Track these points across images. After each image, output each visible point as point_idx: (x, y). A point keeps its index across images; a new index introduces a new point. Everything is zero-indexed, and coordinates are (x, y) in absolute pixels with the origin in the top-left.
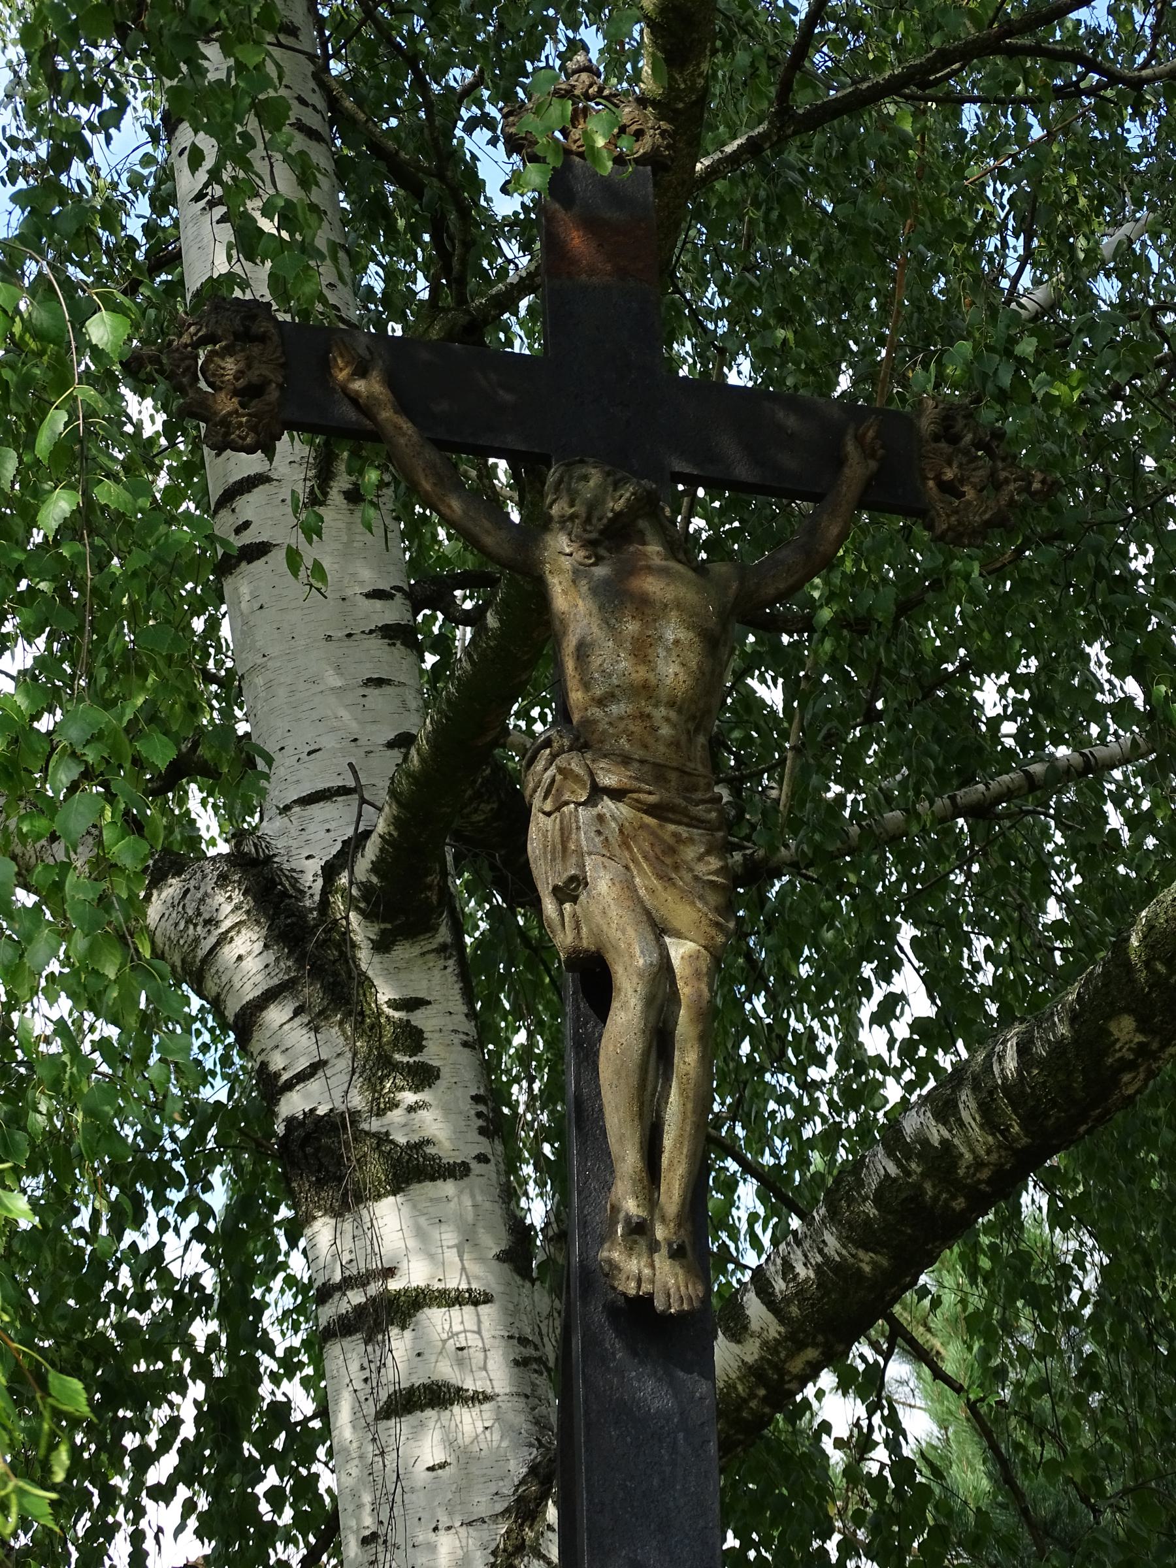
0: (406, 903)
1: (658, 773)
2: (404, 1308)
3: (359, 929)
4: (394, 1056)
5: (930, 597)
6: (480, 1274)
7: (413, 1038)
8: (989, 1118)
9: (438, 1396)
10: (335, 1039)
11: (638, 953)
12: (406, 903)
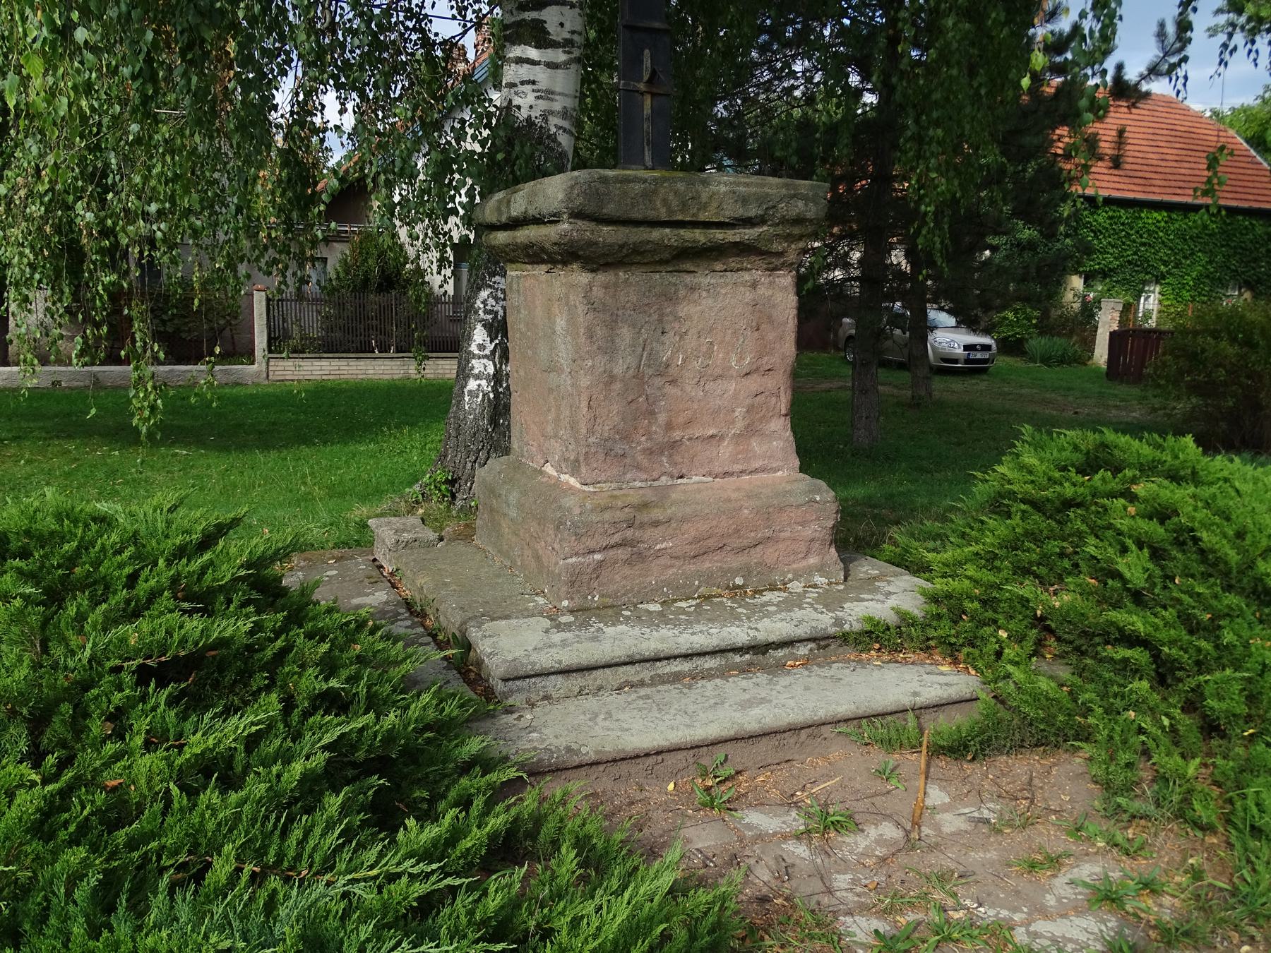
5: (601, 361)
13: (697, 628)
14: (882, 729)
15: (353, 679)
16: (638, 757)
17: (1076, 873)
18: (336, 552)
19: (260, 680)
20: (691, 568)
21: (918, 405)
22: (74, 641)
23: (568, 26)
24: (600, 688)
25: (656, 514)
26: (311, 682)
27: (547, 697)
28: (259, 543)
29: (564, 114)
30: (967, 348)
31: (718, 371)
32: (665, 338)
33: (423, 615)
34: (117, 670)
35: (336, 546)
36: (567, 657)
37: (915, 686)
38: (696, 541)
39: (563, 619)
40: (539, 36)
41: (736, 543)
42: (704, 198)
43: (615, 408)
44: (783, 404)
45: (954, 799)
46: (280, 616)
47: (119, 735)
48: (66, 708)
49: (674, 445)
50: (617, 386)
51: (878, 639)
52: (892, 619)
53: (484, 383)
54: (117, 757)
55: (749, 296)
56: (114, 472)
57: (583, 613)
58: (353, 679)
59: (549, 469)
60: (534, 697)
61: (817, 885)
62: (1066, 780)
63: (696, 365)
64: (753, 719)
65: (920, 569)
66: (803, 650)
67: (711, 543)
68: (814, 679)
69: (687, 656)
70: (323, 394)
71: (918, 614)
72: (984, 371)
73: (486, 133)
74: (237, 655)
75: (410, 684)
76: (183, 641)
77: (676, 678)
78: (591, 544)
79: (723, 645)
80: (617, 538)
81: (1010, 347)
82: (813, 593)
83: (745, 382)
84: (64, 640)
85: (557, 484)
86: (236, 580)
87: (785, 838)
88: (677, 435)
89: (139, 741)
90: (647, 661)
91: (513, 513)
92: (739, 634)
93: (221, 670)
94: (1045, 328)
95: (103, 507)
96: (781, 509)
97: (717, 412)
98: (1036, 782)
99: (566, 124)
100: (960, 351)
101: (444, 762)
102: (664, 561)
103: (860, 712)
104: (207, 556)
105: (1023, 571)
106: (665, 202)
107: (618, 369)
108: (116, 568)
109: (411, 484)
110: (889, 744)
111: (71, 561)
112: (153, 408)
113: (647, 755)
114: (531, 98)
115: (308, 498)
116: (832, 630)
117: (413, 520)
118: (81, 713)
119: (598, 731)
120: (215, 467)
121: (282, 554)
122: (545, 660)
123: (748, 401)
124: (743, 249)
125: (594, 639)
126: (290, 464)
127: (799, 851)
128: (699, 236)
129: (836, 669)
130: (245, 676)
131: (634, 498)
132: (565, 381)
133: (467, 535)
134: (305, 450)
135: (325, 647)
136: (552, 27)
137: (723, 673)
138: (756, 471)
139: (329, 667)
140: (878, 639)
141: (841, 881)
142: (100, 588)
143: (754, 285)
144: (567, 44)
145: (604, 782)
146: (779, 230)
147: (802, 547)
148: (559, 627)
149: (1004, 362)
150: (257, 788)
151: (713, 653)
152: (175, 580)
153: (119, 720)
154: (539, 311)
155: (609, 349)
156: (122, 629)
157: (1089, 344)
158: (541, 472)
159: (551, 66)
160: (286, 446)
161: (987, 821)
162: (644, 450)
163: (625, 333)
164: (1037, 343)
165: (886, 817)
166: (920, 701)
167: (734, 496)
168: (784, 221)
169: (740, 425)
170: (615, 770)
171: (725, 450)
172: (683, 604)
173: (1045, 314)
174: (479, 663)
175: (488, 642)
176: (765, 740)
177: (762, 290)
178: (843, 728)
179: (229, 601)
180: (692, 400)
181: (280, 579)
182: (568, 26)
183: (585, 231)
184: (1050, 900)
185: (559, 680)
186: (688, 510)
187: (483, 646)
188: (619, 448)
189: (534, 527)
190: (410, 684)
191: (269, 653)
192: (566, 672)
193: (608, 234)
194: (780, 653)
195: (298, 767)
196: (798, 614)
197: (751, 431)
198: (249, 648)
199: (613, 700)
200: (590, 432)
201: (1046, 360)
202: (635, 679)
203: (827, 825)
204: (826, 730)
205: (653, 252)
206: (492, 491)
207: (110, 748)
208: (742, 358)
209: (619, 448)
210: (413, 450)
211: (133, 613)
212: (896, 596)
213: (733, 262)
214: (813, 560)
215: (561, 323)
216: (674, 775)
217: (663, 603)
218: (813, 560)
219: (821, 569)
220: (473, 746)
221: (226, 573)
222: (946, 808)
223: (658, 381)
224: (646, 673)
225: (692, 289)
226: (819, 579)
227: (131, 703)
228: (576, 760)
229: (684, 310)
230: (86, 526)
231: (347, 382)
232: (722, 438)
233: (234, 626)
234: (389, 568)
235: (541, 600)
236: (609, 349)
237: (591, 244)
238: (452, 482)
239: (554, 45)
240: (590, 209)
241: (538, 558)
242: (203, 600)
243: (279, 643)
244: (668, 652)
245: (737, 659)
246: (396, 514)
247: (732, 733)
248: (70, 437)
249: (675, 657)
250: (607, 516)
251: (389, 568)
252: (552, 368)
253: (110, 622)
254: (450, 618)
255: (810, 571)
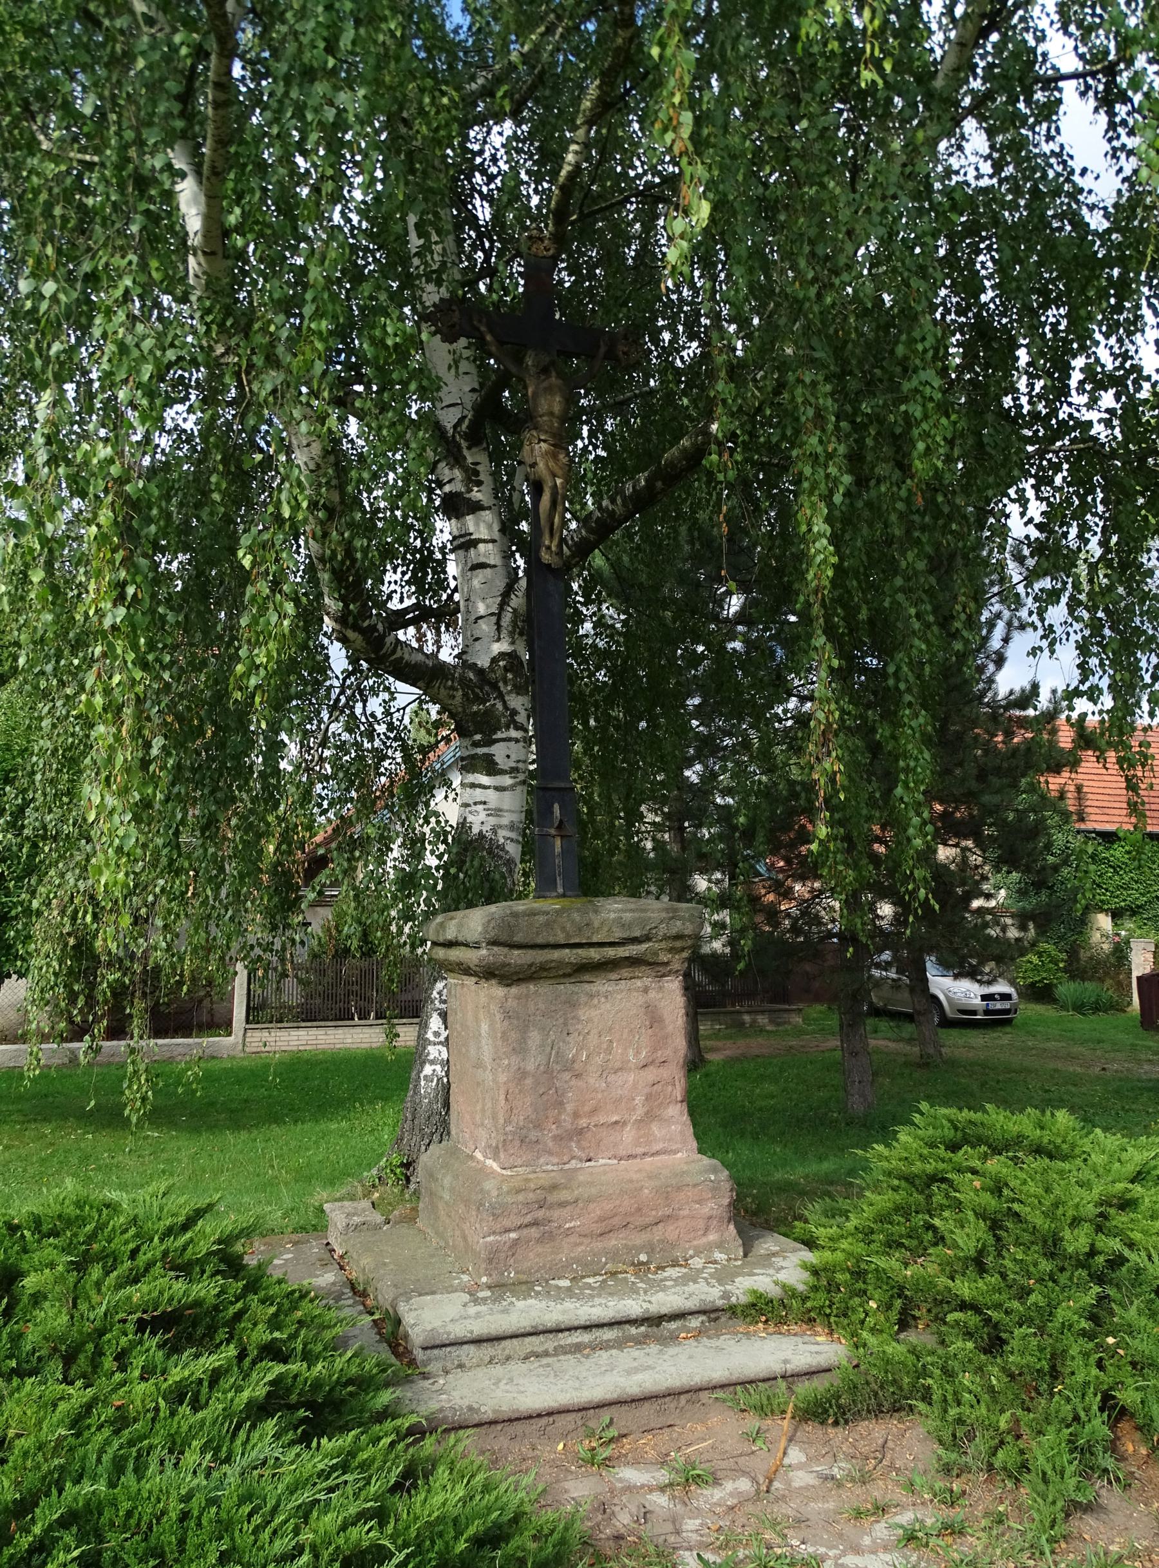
0: (475, 437)
1: (554, 435)
2: (474, 543)
3: (464, 444)
4: (472, 477)
5: (515, 1060)
6: (496, 535)
7: (477, 473)
8: (624, 504)
9: (483, 566)
10: (457, 473)
11: (972, 1115)
12: (475, 437)
13: (597, 1301)
14: (750, 1394)
15: (293, 1336)
16: (530, 1417)
17: (899, 1519)
18: (295, 1237)
19: (221, 1334)
20: (598, 1245)
21: (927, 1065)
22: (95, 1298)
23: (514, 757)
24: (508, 1358)
25: (564, 1195)
26: (262, 1335)
27: (461, 1366)
28: (229, 1222)
29: (512, 827)
30: (984, 998)
31: (618, 1065)
32: (570, 1039)
33: (364, 1294)
34: (124, 1321)
35: (295, 1231)
36: (479, 1328)
37: (788, 1354)
38: (601, 1219)
39: (481, 1294)
40: (491, 768)
41: (640, 1221)
42: (596, 924)
43: (528, 1101)
44: (678, 1092)
45: (809, 1459)
46: (240, 1284)
47: (123, 1368)
48: (90, 1347)
49: (580, 1132)
50: (529, 1081)
51: (762, 1311)
52: (774, 1292)
53: (438, 1068)
54: (123, 1383)
55: (641, 999)
56: (87, 1158)
57: (499, 1288)
58: (293, 1336)
59: (478, 1155)
60: (449, 1365)
61: (669, 1527)
62: (912, 1442)
63: (598, 1060)
64: (635, 1384)
65: (810, 1243)
66: (695, 1322)
67: (616, 1221)
68: (701, 1349)
69: (587, 1328)
70: (299, 1068)
71: (801, 1288)
72: (1008, 1022)
73: (442, 847)
74: (208, 1313)
75: (340, 1344)
76: (171, 1299)
77: (578, 1348)
78: (507, 1223)
79: (619, 1317)
80: (528, 1219)
81: (1040, 993)
82: (711, 1269)
83: (643, 1073)
84: (88, 1298)
85: (482, 1171)
86: (209, 1254)
87: (651, 1490)
88: (583, 1122)
89: (137, 1373)
90: (550, 1331)
91: (447, 1196)
92: (633, 1307)
93: (194, 1325)
94: (1076, 971)
95: (113, 1195)
96: (679, 1189)
97: (619, 1100)
98: (890, 1444)
99: (513, 835)
100: (978, 1001)
101: (362, 1411)
102: (573, 1239)
103: (734, 1378)
104: (188, 1235)
105: (893, 1244)
106: (563, 929)
107: (530, 1066)
108: (122, 1245)
109: (369, 1167)
110: (762, 1410)
111: (92, 1237)
112: (144, 1099)
113: (539, 1416)
114: (482, 816)
115: (272, 1183)
116: (720, 1303)
117: (365, 1204)
118: (99, 1353)
119: (499, 1393)
120: (185, 1149)
121: (246, 1233)
122: (459, 1331)
123: (647, 1090)
124: (634, 962)
125: (505, 1311)
126: (259, 1145)
127: (660, 1501)
128: (594, 954)
129: (722, 1341)
130: (212, 1330)
131: (544, 1180)
132: (488, 1076)
133: (411, 1218)
134: (276, 1130)
135: (272, 1310)
136: (500, 759)
137: (620, 1344)
138: (657, 1153)
139: (274, 1323)
140: (762, 1311)
141: (691, 1524)
142: (110, 1261)
143: (646, 990)
144: (513, 771)
145: (499, 1440)
146: (663, 945)
147: (701, 1224)
148: (476, 1301)
149: (1032, 1011)
150: (215, 1408)
151: (611, 1324)
152: (165, 1254)
153: (122, 1359)
154: (470, 1016)
155: (520, 1049)
156: (129, 1290)
157: (1123, 988)
158: (472, 1157)
159: (497, 789)
160: (256, 1126)
161: (833, 1478)
162: (555, 1138)
163: (535, 1037)
164: (1066, 989)
165: (745, 1473)
166: (790, 1368)
167: (635, 1177)
168: (665, 938)
169: (640, 1111)
170: (512, 1429)
171: (628, 1135)
172: (590, 1280)
173: (1073, 954)
174: (406, 1337)
175: (413, 1314)
176: (647, 1404)
177: (652, 994)
178: (720, 1394)
179: (203, 1272)
180: (595, 1090)
181: (241, 1257)
182: (514, 757)
183: (500, 954)
184: (867, 1541)
185: (472, 1348)
186: (594, 1191)
187: (408, 1319)
188: (533, 1135)
189: (461, 1209)
190: (340, 1344)
191: (232, 1310)
192: (478, 1341)
193: (518, 957)
194: (673, 1325)
195: (246, 1394)
196: (691, 1287)
197: (650, 1116)
198: (216, 1308)
199: (516, 1367)
200: (508, 1121)
201: (1079, 1008)
202: (540, 1349)
203: (691, 1479)
204: (704, 1396)
205: (557, 968)
206: (431, 1175)
207: (118, 1377)
208: (638, 1053)
209: (533, 1135)
210: (376, 1129)
211: (134, 1279)
212: (785, 1267)
213: (625, 972)
214: (712, 1237)
215: (485, 1027)
216: (565, 1436)
217: (573, 1280)
218: (712, 1237)
219: (720, 1246)
220: (385, 1397)
221: (203, 1247)
222: (800, 1466)
223: (566, 1076)
224: (550, 1343)
225: (592, 996)
226: (719, 1256)
227: (133, 1345)
228: (476, 1418)
229: (583, 1013)
230: (100, 1211)
231: (324, 1052)
232: (625, 1123)
233: (206, 1289)
234: (339, 1251)
235: (465, 1278)
236: (520, 1049)
237: (504, 965)
238: (407, 1165)
239: (502, 772)
240: (504, 938)
241: (465, 1238)
242: (185, 1268)
243: (239, 1305)
244: (568, 1324)
245: (633, 1331)
246: (352, 1198)
247: (614, 1396)
248: (46, 1120)
249: (576, 1328)
250: (521, 1197)
251: (339, 1251)
252: (479, 1065)
253: (119, 1286)
254: (384, 1294)
255: (710, 1247)
